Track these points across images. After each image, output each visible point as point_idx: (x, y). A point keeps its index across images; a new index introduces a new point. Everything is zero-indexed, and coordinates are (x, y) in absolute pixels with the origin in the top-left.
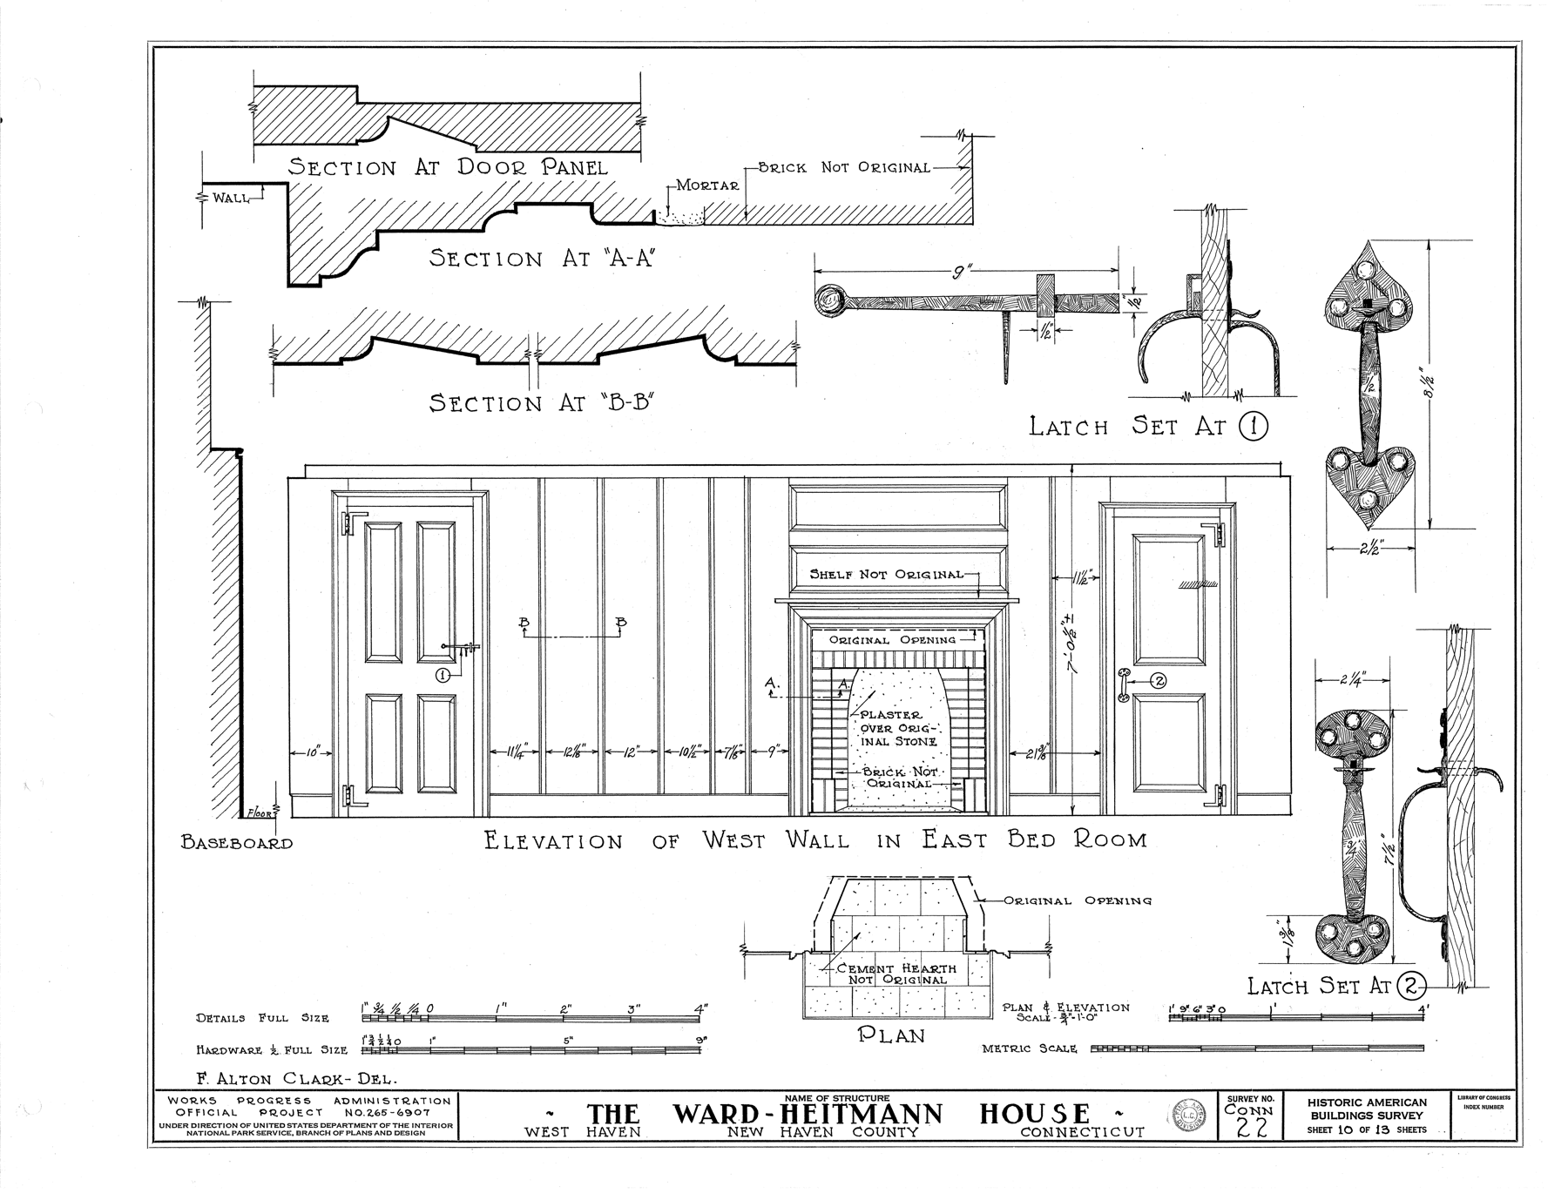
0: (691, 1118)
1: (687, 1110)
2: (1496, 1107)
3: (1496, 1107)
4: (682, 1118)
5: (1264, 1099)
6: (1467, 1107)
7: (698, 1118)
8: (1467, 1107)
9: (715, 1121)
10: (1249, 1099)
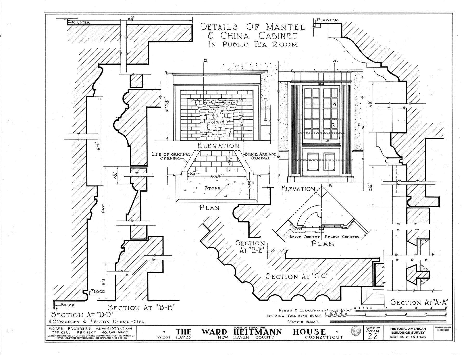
0: (207, 333)
1: (206, 330)
2: (447, 330)
3: (447, 330)
4: (204, 333)
5: (377, 328)
6: (438, 330)
7: (209, 333)
8: (438, 330)
9: (214, 334)
10: (373, 328)
